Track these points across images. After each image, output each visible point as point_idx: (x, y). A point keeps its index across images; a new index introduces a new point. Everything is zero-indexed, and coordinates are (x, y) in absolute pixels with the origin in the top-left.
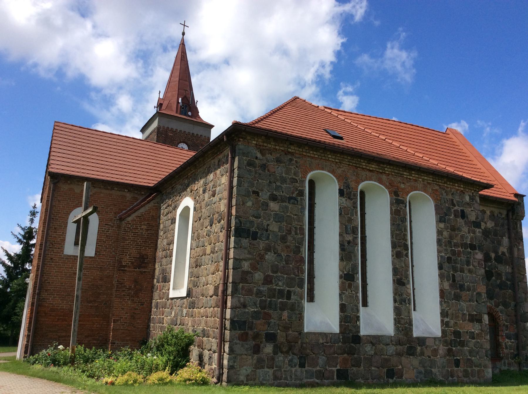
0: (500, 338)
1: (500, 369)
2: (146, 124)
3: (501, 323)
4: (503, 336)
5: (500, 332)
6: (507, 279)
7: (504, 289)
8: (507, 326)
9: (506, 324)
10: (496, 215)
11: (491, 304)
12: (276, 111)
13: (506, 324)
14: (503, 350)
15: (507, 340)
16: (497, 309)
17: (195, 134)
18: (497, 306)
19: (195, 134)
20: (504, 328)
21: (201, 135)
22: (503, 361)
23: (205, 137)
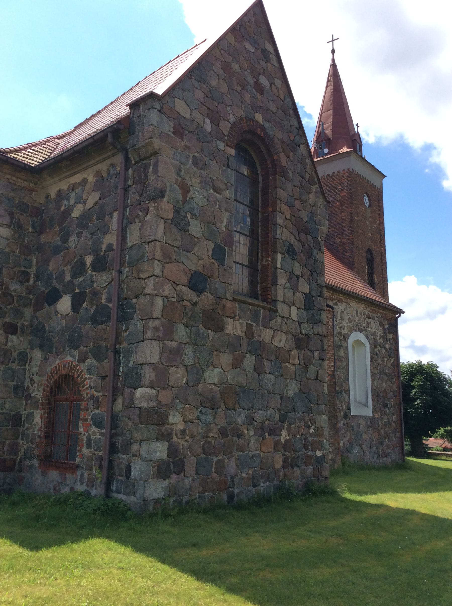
0: (80, 423)
1: (72, 489)
2: (380, 172)
3: (86, 393)
4: (87, 420)
5: (82, 413)
6: (109, 300)
7: (103, 323)
8: (97, 400)
9: (96, 394)
10: (104, 174)
11: (73, 357)
12: (21, 150)
13: (96, 394)
14: (80, 451)
15: (94, 429)
16: (83, 366)
17: (331, 174)
18: (82, 360)
19: (331, 174)
20: (91, 404)
21: (339, 172)
22: (79, 473)
23: (344, 170)
